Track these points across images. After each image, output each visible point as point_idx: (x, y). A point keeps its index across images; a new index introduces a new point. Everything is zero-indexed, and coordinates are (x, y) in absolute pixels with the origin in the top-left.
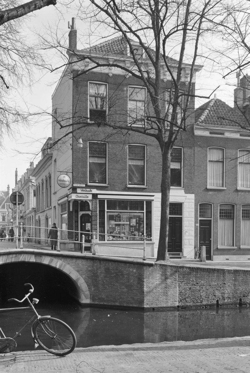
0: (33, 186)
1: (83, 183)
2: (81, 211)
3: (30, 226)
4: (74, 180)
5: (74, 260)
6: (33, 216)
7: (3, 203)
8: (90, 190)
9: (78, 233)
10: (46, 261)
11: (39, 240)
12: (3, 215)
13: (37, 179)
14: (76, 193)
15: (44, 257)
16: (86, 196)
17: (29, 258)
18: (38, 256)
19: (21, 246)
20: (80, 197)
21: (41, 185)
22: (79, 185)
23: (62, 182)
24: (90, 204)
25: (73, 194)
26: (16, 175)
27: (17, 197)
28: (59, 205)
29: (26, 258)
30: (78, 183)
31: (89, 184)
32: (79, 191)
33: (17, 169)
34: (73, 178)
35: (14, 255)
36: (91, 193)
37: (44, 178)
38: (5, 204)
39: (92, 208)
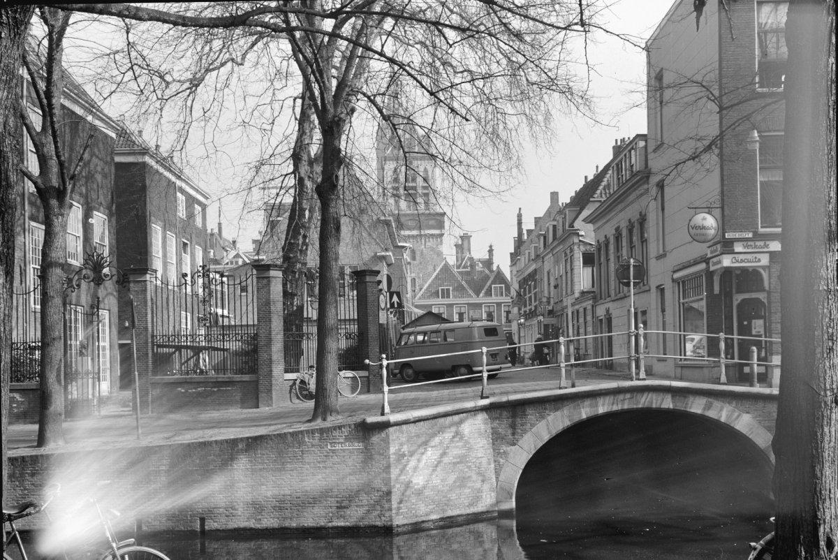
0: (581, 243)
1: (747, 230)
2: (738, 292)
3: (682, 333)
4: (724, 225)
5: (760, 404)
6: (585, 309)
7: (488, 284)
8: (765, 245)
9: (732, 339)
10: (696, 406)
11: (611, 362)
12: (487, 310)
13: (598, 228)
14: (733, 252)
15: (691, 398)
16: (756, 258)
17: (659, 402)
18: (680, 396)
19: (642, 375)
20: (742, 261)
21: (612, 240)
22: (737, 235)
23: (699, 231)
24: (765, 275)
25: (724, 256)
26: (520, 223)
27: (632, 269)
28: (673, 280)
29: (654, 401)
30: (735, 229)
31: (761, 230)
32: (738, 248)
33: (520, 209)
34: (723, 220)
35: (628, 396)
36: (766, 250)
37: (624, 225)
38: (493, 286)
39: (770, 283)
